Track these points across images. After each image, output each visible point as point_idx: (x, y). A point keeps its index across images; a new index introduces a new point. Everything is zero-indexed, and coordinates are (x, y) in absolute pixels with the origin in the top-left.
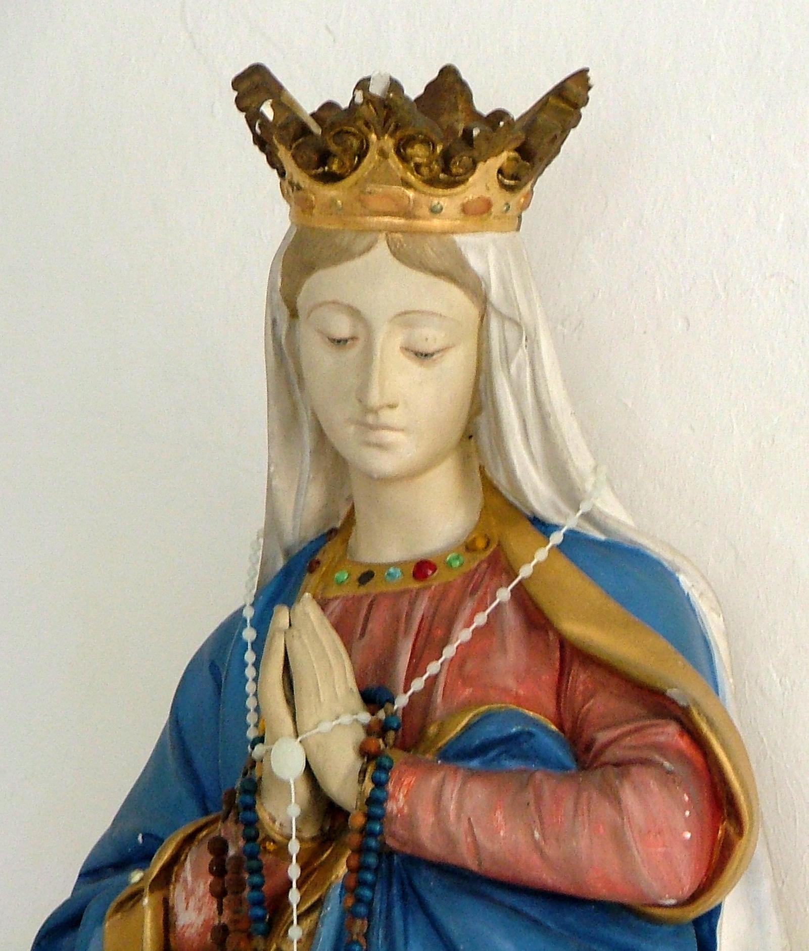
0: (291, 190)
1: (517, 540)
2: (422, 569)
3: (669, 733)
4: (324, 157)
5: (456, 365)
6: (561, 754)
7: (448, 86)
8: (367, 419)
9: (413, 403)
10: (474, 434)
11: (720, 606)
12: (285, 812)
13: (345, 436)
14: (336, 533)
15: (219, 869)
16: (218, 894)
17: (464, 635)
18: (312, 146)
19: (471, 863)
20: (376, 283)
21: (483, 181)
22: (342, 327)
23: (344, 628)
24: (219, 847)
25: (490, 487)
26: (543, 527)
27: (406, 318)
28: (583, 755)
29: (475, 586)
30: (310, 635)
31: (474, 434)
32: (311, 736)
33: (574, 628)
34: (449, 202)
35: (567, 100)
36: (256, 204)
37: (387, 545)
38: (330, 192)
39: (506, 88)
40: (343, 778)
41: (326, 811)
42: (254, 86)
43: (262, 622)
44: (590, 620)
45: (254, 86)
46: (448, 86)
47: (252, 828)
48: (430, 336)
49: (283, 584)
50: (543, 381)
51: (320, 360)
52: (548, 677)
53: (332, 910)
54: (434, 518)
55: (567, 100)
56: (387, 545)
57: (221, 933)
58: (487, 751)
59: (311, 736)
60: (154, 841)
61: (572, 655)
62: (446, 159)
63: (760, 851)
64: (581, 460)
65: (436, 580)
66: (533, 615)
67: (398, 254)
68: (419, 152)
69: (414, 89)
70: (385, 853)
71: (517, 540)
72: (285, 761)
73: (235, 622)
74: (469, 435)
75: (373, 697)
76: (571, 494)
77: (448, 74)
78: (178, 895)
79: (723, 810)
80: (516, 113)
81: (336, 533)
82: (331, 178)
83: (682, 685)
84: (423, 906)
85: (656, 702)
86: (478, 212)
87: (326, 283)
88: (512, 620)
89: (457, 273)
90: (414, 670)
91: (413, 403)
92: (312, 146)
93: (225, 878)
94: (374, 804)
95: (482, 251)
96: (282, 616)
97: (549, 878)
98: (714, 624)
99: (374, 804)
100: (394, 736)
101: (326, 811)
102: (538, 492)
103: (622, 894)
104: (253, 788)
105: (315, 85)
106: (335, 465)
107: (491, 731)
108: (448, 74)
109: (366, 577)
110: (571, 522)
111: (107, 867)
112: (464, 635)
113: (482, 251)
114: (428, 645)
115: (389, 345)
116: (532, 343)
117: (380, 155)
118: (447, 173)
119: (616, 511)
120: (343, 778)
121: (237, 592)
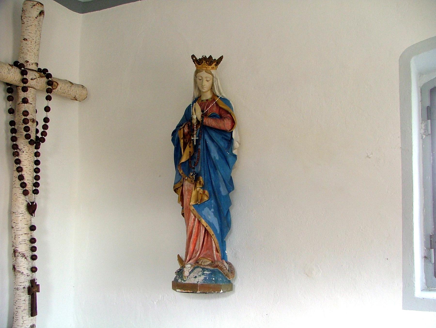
0: (196, 66)
1: (216, 98)
2: (207, 100)
3: (229, 115)
4: (199, 63)
5: (211, 82)
6: (219, 116)
7: (210, 57)
8: (202, 87)
9: (207, 85)
10: (212, 88)
11: (234, 104)
12: (194, 121)
13: (201, 88)
14: (199, 97)
15: (188, 126)
16: (188, 129)
17: (211, 106)
18: (198, 62)
19: (210, 126)
20: (204, 74)
21: (213, 65)
22: (200, 78)
23: (200, 105)
24: (188, 124)
25: (213, 93)
26: (218, 97)
27: (206, 77)
28: (221, 117)
29: (212, 102)
30: (197, 106)
31: (212, 88)
32: (197, 115)
33: (221, 106)
34: (210, 67)
35: (221, 58)
36: (193, 67)
37: (204, 98)
38: (200, 66)
39: (216, 57)
40: (200, 118)
41: (198, 121)
42: (193, 56)
43: (193, 105)
44: (222, 105)
45: (193, 56)
46: (210, 57)
47: (191, 123)
48: (208, 79)
49: (194, 102)
50: (218, 84)
51: (198, 81)
52: (218, 110)
53: (198, 132)
54: (208, 96)
55: (221, 58)
56: (204, 98)
57: (188, 132)
58: (213, 116)
59: (197, 115)
60: (183, 124)
61: (220, 108)
62: (210, 63)
63: (237, 126)
64: (222, 91)
65: (208, 101)
66: (217, 104)
67: (206, 72)
68: (208, 62)
69: (37, 284)
70: (203, 125)
71: (216, 98)
72: (194, 117)
73: (190, 105)
74: (212, 88)
75: (202, 111)
76: (221, 94)
77: (211, 56)
78: (185, 129)
79: (233, 123)
80: (42, 144)
81: (199, 97)
82: (200, 65)
83: (230, 111)
84: (207, 131)
85: (228, 112)
86: (213, 68)
87: (199, 74)
88: (215, 105)
89: (211, 74)
90: (206, 109)
91: (207, 85)
92: (198, 62)
93: (189, 127)
94: (202, 121)
95: (213, 72)
96: (194, 104)
97: (217, 127)
98: (233, 106)
99: (202, 121)
100: (204, 115)
101: (198, 121)
102: (218, 94)
103: (224, 129)
104: (192, 119)
105: (199, 57)
106: (200, 91)
107: (213, 115)
108: (211, 56)
109: (202, 101)
110: (221, 96)
111: (178, 127)
112: (211, 106)
113: (213, 72)
114: (207, 107)
115: (205, 80)
116: (217, 80)
117: (205, 63)
118: (210, 64)
119: (225, 96)
120: (200, 118)
121: (191, 103)
